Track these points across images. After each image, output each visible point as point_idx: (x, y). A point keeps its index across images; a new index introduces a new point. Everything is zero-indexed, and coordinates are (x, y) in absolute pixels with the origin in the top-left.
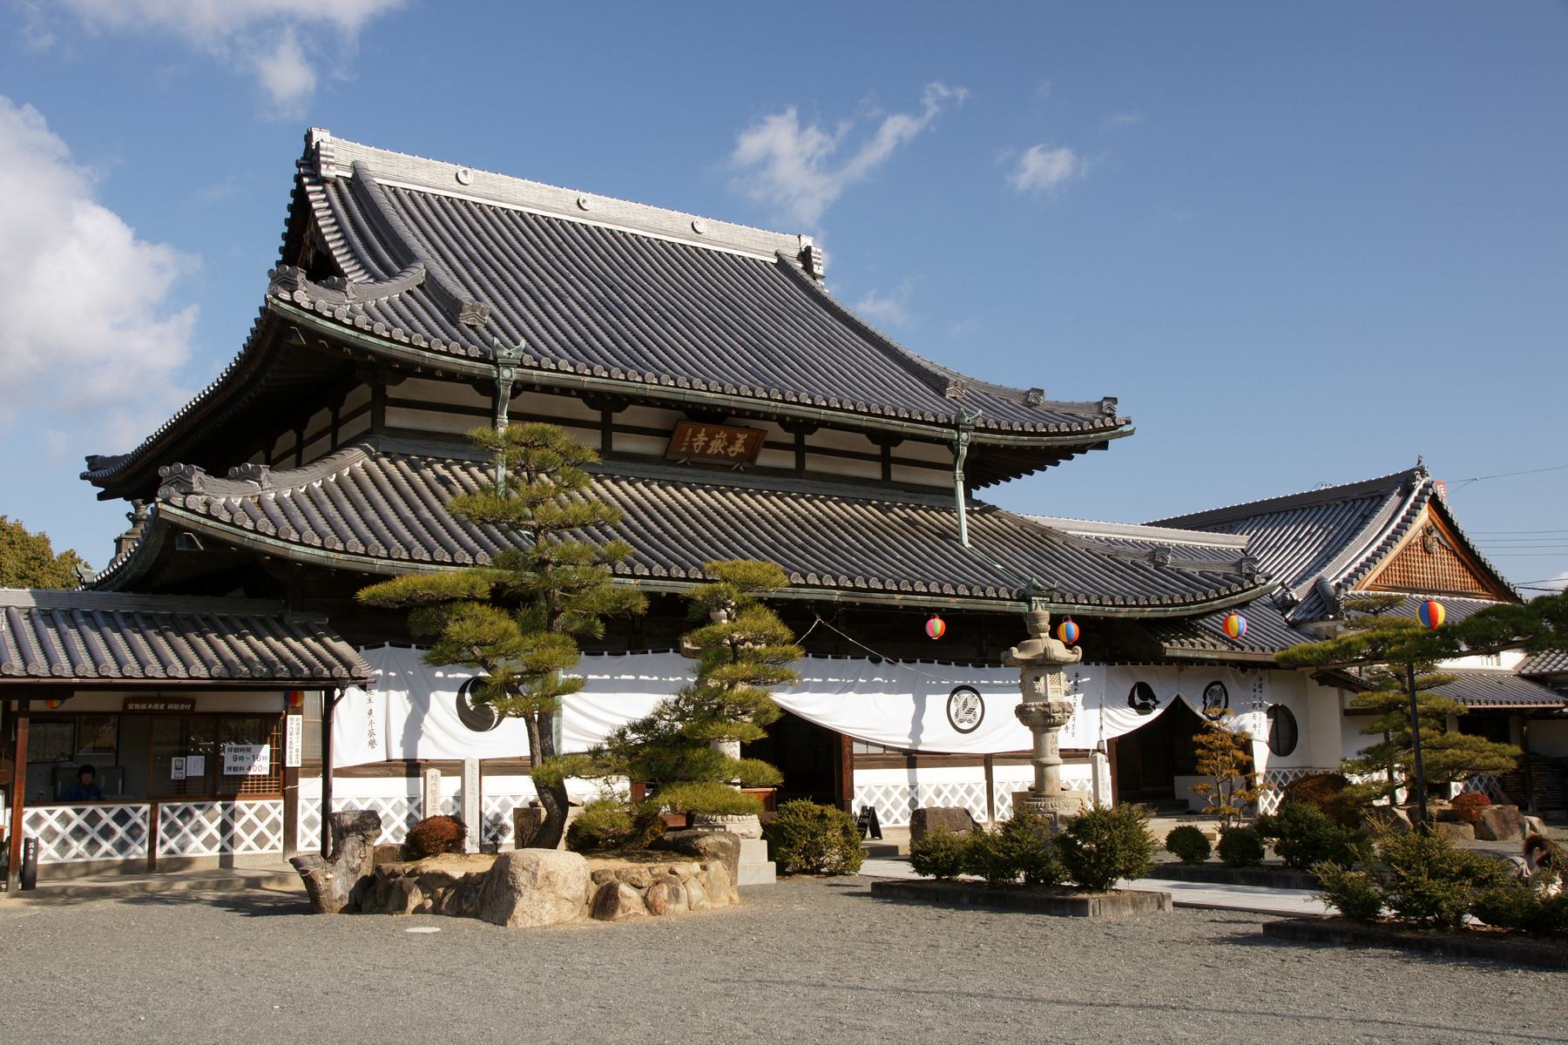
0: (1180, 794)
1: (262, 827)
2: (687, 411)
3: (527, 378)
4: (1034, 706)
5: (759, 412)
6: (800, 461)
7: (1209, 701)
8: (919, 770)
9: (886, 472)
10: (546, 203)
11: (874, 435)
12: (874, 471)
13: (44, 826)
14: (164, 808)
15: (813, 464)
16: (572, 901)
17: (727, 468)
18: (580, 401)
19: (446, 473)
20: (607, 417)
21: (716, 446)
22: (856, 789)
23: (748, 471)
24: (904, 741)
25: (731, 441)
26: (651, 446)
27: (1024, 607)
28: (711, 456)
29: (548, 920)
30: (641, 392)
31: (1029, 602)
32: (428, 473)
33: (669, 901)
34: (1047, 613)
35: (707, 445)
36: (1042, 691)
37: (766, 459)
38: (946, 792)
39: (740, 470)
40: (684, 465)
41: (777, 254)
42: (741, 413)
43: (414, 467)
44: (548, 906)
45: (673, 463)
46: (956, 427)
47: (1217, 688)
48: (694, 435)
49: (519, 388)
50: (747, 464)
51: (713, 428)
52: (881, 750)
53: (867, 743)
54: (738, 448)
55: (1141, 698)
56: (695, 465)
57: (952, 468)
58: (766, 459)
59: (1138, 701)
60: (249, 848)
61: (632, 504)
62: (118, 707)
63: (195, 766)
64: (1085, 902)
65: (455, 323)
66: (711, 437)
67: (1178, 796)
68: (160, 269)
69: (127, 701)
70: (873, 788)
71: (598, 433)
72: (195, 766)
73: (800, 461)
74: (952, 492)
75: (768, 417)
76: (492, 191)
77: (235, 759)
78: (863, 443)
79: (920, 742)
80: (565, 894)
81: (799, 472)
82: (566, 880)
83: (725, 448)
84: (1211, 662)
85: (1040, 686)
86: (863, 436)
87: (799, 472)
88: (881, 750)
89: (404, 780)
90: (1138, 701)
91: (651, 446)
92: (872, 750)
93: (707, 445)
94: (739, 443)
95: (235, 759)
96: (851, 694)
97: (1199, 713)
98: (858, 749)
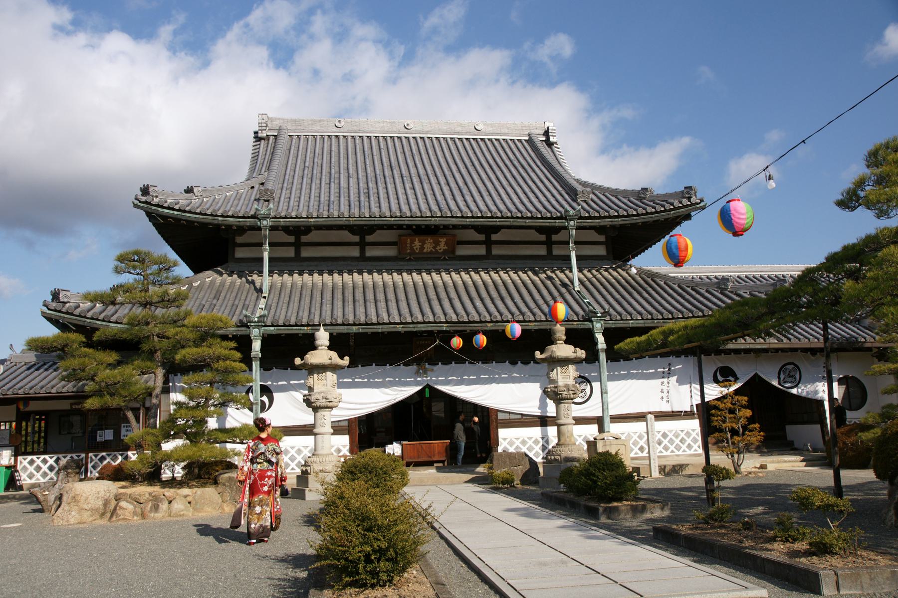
0: (790, 437)
1: (689, 441)
2: (413, 230)
3: (277, 224)
4: (550, 387)
5: (402, 225)
6: (489, 250)
7: (782, 376)
8: (549, 428)
9: (549, 250)
10: (386, 129)
11: (540, 230)
12: (542, 251)
13: (35, 465)
14: (90, 455)
15: (496, 251)
16: (91, 510)
17: (438, 259)
18: (346, 232)
19: (553, 275)
20: (362, 238)
21: (428, 247)
22: (500, 440)
23: (451, 259)
24: (538, 413)
25: (437, 243)
26: (391, 252)
27: (588, 325)
28: (427, 253)
29: (72, 521)
30: (347, 223)
31: (591, 321)
32: (543, 276)
33: (151, 511)
34: (563, 329)
35: (422, 248)
36: (555, 378)
37: (462, 251)
38: (671, 436)
39: (448, 260)
40: (410, 260)
41: (529, 135)
42: (446, 227)
43: (536, 273)
44: (73, 513)
45: (403, 259)
46: (565, 219)
47: (790, 367)
48: (412, 242)
49: (273, 228)
50: (451, 256)
51: (422, 237)
52: (519, 417)
53: (509, 413)
54: (442, 247)
55: (724, 375)
56: (417, 259)
57: (261, 245)
58: (462, 251)
59: (720, 378)
60: (293, 469)
61: (623, 281)
62: (68, 407)
63: (109, 435)
64: (616, 508)
65: (575, 201)
66: (423, 243)
67: (788, 439)
68: (238, 196)
69: (72, 404)
70: (509, 439)
71: (484, 246)
72: (109, 435)
73: (489, 250)
74: (568, 258)
75: (465, 227)
76: (355, 128)
77: (127, 431)
78: (346, 236)
79: (547, 412)
80: (85, 506)
81: (488, 256)
82: (87, 499)
83: (434, 248)
84: (783, 350)
85: (553, 375)
86: (533, 231)
87: (488, 256)
88: (519, 417)
89: (539, 428)
90: (720, 378)
91: (391, 252)
92: (513, 417)
93: (422, 248)
94: (442, 244)
95: (127, 431)
96: (494, 384)
97: (775, 383)
98: (501, 416)
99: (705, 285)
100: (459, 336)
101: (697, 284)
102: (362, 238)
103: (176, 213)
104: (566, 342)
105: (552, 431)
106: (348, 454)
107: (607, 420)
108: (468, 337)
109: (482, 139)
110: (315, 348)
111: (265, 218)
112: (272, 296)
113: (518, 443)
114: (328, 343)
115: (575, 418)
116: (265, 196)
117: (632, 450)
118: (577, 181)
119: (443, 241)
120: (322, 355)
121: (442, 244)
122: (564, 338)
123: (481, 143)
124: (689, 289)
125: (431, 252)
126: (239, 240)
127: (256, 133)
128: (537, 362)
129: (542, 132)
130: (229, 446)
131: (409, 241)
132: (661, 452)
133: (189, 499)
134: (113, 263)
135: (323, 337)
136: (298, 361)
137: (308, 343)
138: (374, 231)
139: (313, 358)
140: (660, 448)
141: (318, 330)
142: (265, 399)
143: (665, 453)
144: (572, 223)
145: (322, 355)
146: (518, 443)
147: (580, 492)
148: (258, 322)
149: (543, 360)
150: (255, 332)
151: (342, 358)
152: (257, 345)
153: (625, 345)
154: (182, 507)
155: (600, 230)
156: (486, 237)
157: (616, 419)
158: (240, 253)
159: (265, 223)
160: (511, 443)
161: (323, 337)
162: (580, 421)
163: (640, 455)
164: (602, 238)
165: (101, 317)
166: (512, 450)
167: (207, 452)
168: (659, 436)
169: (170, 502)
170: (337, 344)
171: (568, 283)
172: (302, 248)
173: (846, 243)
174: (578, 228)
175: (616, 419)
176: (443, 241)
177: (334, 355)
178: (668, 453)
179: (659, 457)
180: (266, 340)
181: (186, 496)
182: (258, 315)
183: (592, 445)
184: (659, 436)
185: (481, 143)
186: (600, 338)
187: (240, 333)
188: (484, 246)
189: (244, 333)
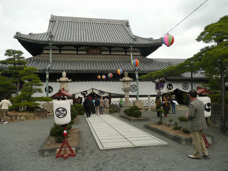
22: (111, 101)
23: (100, 55)
26: (85, 53)
28: (94, 53)
33: (15, 119)
40: (90, 55)
45: (88, 54)
71: (59, 51)
78: (73, 48)
99: (164, 63)
100: (104, 75)
101: (163, 63)
102: (110, 49)
103: (26, 40)
104: (128, 77)
105: (124, 99)
106: (72, 104)
107: (138, 96)
108: (107, 75)
109: (114, 24)
110: (62, 77)
111: (50, 42)
112: (50, 63)
113: (116, 102)
114: (66, 75)
115: (129, 95)
116: (51, 36)
117: (151, 104)
118: (134, 35)
119: (98, 50)
120: (64, 78)
121: (98, 51)
122: (127, 75)
123: (110, 25)
124: (160, 64)
125: (95, 53)
126: (44, 48)
127: (50, 20)
128: (120, 81)
129: (126, 22)
130: (37, 102)
131: (89, 50)
132: (152, 105)
133: (26, 116)
134: (5, 52)
135: (64, 74)
136: (58, 80)
137: (60, 76)
138: (81, 47)
139: (62, 79)
140: (152, 104)
141: (63, 72)
142: (50, 90)
143: (153, 105)
144: (131, 46)
145: (64, 78)
146: (116, 102)
147: (129, 115)
148: (48, 70)
149: (122, 81)
150: (47, 72)
151: (69, 80)
152: (47, 76)
153: (142, 77)
154: (24, 118)
155: (139, 48)
156: (61, 48)
157: (141, 96)
158: (45, 52)
159: (50, 43)
160: (114, 102)
161: (64, 74)
162: (131, 96)
163: (147, 105)
164: (139, 51)
165: (5, 67)
166: (114, 104)
167: (31, 104)
168: (151, 101)
169: (20, 117)
170: (69, 75)
171: (129, 60)
172: (79, 51)
173: (15, 50)
174: (133, 48)
175: (141, 96)
176: (98, 50)
177: (67, 79)
178: (154, 105)
179: (151, 106)
180: (50, 74)
181: (25, 115)
182: (48, 68)
183: (134, 102)
184: (151, 101)
185: (117, 25)
186: (137, 76)
187: (43, 73)
188: (59, 51)
189: (44, 73)
